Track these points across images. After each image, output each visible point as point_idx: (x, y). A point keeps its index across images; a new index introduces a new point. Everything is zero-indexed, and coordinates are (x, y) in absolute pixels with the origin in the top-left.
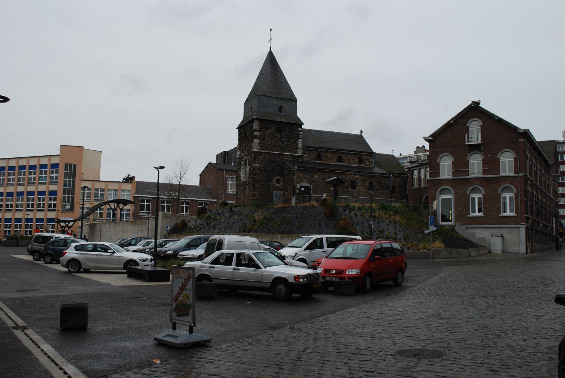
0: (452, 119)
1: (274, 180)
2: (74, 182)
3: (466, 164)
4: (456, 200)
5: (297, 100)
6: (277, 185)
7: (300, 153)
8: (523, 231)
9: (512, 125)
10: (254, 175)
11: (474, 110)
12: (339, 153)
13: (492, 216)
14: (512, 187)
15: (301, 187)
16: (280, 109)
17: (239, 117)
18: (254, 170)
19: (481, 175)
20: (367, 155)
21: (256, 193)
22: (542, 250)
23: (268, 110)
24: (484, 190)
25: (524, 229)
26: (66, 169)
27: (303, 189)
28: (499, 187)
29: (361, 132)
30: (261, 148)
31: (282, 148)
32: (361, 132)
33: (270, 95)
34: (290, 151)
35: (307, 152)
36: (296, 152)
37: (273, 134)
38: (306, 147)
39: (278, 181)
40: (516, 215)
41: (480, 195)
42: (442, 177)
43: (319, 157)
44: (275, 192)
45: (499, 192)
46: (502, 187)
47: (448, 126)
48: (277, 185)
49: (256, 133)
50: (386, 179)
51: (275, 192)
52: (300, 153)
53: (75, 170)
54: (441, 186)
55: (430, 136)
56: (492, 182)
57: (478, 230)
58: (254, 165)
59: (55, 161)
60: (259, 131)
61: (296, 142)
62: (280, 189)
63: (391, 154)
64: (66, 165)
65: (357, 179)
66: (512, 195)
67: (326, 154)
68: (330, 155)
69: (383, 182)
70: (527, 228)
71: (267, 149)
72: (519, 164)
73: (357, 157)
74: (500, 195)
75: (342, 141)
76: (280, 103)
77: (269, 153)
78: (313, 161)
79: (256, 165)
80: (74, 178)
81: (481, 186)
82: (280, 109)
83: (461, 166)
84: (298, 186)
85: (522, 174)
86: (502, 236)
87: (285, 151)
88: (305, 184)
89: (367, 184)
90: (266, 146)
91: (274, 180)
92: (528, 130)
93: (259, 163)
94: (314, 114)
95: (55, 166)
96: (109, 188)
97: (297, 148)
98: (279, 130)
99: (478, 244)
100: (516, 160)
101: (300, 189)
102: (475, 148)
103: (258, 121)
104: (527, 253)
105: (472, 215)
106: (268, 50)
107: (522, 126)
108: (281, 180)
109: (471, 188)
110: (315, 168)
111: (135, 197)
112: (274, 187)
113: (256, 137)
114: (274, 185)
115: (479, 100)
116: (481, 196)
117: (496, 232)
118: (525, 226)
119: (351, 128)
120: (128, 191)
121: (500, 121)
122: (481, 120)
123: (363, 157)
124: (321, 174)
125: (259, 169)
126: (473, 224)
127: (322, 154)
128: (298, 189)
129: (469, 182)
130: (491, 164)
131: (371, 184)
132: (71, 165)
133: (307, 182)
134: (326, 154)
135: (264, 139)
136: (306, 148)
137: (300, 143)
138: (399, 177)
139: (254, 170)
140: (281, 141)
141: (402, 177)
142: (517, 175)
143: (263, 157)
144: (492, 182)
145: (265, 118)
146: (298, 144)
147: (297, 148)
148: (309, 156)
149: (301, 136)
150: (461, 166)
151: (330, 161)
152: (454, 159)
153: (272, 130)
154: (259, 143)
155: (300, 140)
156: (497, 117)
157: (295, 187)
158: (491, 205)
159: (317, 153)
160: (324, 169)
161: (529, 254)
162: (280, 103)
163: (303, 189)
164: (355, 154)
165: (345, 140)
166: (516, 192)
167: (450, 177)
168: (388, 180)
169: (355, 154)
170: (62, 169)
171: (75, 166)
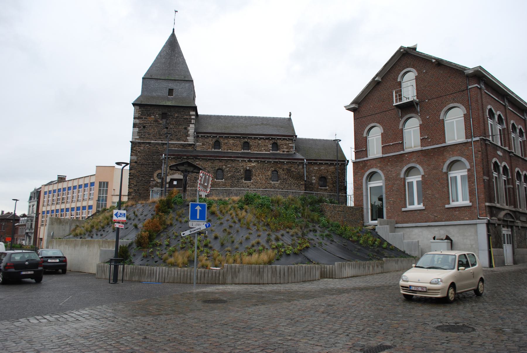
0: (377, 75)
1: (155, 175)
2: (106, 197)
3: (400, 135)
4: (387, 186)
5: (193, 81)
7: (191, 140)
8: (482, 230)
9: (456, 65)
11: (406, 57)
12: (244, 138)
13: (438, 209)
14: (463, 160)
15: (172, 180)
16: (171, 92)
19: (419, 148)
20: (284, 139)
22: (208, 283)
23: (154, 94)
24: (424, 170)
25: (485, 226)
26: (100, 186)
27: (175, 183)
28: (444, 163)
30: (140, 138)
34: (178, 139)
37: (156, 121)
40: (470, 204)
41: (419, 178)
42: (371, 156)
43: (217, 144)
45: (445, 170)
46: (448, 162)
47: (375, 85)
50: (298, 165)
52: (191, 140)
53: (107, 187)
54: (368, 169)
55: (352, 103)
56: (435, 154)
57: (416, 231)
59: (93, 180)
61: (186, 128)
64: (100, 183)
65: (254, 167)
66: (464, 172)
67: (226, 141)
69: (293, 169)
70: (488, 224)
71: (148, 138)
72: (474, 124)
73: (271, 142)
74: (446, 174)
75: (256, 125)
76: (171, 85)
77: (149, 143)
78: (209, 150)
80: (107, 194)
81: (420, 164)
82: (171, 92)
83: (393, 138)
85: (478, 139)
86: (448, 238)
90: (147, 135)
92: (480, 67)
94: (217, 97)
95: (92, 184)
97: (188, 135)
98: (164, 116)
99: (407, 252)
100: (466, 117)
102: (408, 108)
104: (491, 266)
105: (410, 207)
107: (468, 61)
109: (405, 169)
110: (191, 156)
114: (154, 181)
115: (416, 45)
116: (420, 179)
117: (442, 232)
118: (485, 221)
119: (278, 112)
121: (440, 64)
122: (413, 67)
123: (279, 142)
125: (136, 162)
126: (413, 222)
127: (221, 140)
129: (401, 158)
130: (433, 130)
132: (104, 183)
134: (226, 141)
135: (144, 127)
136: (198, 135)
137: (191, 129)
138: (332, 164)
140: (167, 128)
142: (469, 140)
143: (142, 148)
144: (435, 154)
146: (188, 131)
147: (188, 135)
148: (203, 144)
149: (193, 121)
150: (393, 138)
151: (232, 147)
152: (384, 130)
153: (155, 116)
154: (138, 133)
155: (191, 126)
156: (435, 58)
158: (436, 188)
159: (214, 140)
160: (204, 156)
161: (495, 268)
162: (171, 85)
165: (262, 124)
166: (469, 167)
167: (380, 155)
168: (301, 167)
169: (267, 139)
170: (97, 185)
171: (107, 183)
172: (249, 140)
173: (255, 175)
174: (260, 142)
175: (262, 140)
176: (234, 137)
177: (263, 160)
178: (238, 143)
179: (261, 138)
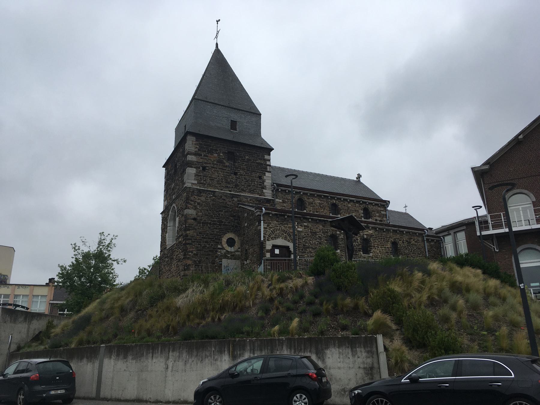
1: (224, 240)
6: (229, 249)
7: (268, 194)
10: (186, 229)
12: (333, 198)
15: (275, 247)
17: (168, 147)
18: (185, 221)
20: (376, 205)
21: (189, 262)
27: (277, 251)
29: (359, 176)
30: (199, 183)
31: (236, 186)
32: (359, 176)
33: (216, 102)
34: (251, 192)
35: (280, 194)
36: (262, 194)
37: (220, 162)
38: (278, 185)
39: (231, 242)
44: (225, 262)
48: (229, 249)
49: (190, 158)
51: (225, 262)
52: (268, 194)
55: (484, 164)
58: (186, 211)
60: (195, 154)
61: (260, 178)
62: (233, 257)
63: (403, 211)
65: (371, 235)
67: (311, 200)
68: (318, 201)
71: (209, 185)
76: (235, 116)
79: (190, 212)
82: (234, 125)
84: (269, 245)
87: (243, 191)
88: (280, 242)
89: (389, 245)
90: (208, 181)
91: (224, 240)
93: (195, 208)
96: (16, 293)
97: (264, 187)
98: (231, 156)
101: (272, 251)
103: (194, 139)
106: (214, 48)
108: (236, 239)
111: (52, 304)
112: (223, 252)
113: (190, 164)
114: (223, 248)
120: (42, 296)
123: (370, 207)
124: (310, 225)
125: (195, 219)
128: (268, 251)
131: (394, 244)
133: (286, 238)
135: (204, 169)
139: (185, 221)
140: (236, 174)
141: (433, 240)
143: (203, 199)
145: (206, 133)
146: (264, 181)
147: (264, 187)
148: (284, 202)
153: (219, 154)
154: (196, 175)
157: (262, 245)
159: (297, 197)
162: (235, 116)
163: (277, 251)
164: (358, 202)
169: (358, 202)
172: (337, 202)
173: (374, 247)
174: (350, 205)
175: (352, 203)
176: (321, 196)
177: (381, 227)
178: (325, 204)
179: (351, 201)
